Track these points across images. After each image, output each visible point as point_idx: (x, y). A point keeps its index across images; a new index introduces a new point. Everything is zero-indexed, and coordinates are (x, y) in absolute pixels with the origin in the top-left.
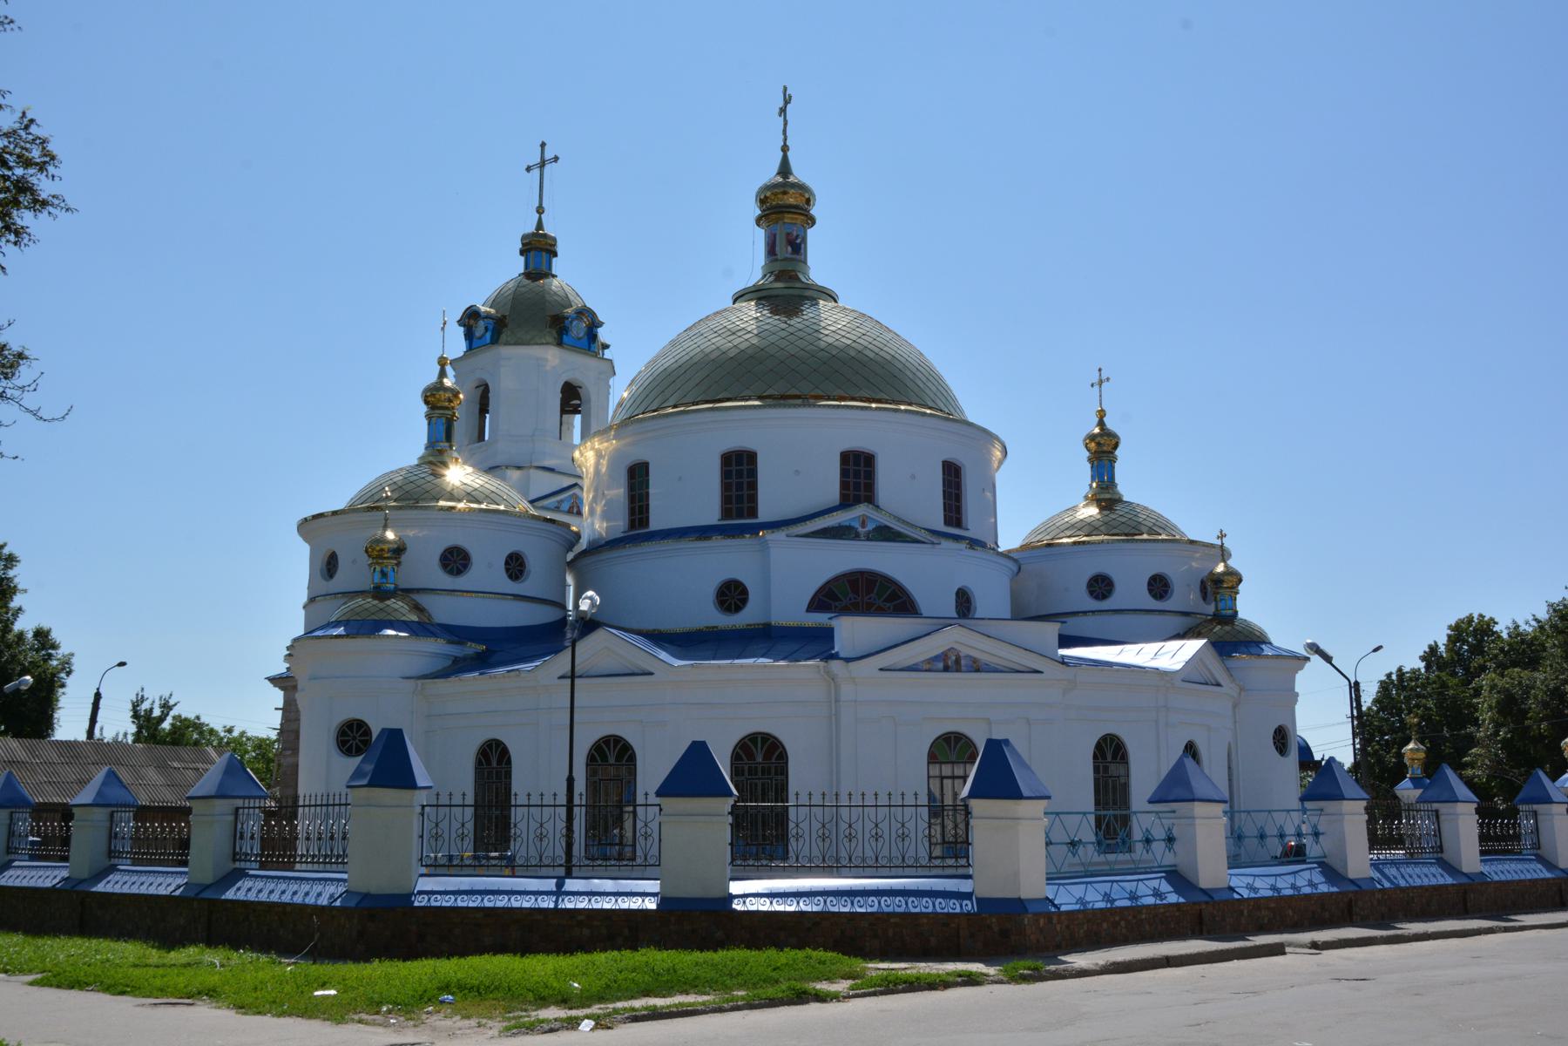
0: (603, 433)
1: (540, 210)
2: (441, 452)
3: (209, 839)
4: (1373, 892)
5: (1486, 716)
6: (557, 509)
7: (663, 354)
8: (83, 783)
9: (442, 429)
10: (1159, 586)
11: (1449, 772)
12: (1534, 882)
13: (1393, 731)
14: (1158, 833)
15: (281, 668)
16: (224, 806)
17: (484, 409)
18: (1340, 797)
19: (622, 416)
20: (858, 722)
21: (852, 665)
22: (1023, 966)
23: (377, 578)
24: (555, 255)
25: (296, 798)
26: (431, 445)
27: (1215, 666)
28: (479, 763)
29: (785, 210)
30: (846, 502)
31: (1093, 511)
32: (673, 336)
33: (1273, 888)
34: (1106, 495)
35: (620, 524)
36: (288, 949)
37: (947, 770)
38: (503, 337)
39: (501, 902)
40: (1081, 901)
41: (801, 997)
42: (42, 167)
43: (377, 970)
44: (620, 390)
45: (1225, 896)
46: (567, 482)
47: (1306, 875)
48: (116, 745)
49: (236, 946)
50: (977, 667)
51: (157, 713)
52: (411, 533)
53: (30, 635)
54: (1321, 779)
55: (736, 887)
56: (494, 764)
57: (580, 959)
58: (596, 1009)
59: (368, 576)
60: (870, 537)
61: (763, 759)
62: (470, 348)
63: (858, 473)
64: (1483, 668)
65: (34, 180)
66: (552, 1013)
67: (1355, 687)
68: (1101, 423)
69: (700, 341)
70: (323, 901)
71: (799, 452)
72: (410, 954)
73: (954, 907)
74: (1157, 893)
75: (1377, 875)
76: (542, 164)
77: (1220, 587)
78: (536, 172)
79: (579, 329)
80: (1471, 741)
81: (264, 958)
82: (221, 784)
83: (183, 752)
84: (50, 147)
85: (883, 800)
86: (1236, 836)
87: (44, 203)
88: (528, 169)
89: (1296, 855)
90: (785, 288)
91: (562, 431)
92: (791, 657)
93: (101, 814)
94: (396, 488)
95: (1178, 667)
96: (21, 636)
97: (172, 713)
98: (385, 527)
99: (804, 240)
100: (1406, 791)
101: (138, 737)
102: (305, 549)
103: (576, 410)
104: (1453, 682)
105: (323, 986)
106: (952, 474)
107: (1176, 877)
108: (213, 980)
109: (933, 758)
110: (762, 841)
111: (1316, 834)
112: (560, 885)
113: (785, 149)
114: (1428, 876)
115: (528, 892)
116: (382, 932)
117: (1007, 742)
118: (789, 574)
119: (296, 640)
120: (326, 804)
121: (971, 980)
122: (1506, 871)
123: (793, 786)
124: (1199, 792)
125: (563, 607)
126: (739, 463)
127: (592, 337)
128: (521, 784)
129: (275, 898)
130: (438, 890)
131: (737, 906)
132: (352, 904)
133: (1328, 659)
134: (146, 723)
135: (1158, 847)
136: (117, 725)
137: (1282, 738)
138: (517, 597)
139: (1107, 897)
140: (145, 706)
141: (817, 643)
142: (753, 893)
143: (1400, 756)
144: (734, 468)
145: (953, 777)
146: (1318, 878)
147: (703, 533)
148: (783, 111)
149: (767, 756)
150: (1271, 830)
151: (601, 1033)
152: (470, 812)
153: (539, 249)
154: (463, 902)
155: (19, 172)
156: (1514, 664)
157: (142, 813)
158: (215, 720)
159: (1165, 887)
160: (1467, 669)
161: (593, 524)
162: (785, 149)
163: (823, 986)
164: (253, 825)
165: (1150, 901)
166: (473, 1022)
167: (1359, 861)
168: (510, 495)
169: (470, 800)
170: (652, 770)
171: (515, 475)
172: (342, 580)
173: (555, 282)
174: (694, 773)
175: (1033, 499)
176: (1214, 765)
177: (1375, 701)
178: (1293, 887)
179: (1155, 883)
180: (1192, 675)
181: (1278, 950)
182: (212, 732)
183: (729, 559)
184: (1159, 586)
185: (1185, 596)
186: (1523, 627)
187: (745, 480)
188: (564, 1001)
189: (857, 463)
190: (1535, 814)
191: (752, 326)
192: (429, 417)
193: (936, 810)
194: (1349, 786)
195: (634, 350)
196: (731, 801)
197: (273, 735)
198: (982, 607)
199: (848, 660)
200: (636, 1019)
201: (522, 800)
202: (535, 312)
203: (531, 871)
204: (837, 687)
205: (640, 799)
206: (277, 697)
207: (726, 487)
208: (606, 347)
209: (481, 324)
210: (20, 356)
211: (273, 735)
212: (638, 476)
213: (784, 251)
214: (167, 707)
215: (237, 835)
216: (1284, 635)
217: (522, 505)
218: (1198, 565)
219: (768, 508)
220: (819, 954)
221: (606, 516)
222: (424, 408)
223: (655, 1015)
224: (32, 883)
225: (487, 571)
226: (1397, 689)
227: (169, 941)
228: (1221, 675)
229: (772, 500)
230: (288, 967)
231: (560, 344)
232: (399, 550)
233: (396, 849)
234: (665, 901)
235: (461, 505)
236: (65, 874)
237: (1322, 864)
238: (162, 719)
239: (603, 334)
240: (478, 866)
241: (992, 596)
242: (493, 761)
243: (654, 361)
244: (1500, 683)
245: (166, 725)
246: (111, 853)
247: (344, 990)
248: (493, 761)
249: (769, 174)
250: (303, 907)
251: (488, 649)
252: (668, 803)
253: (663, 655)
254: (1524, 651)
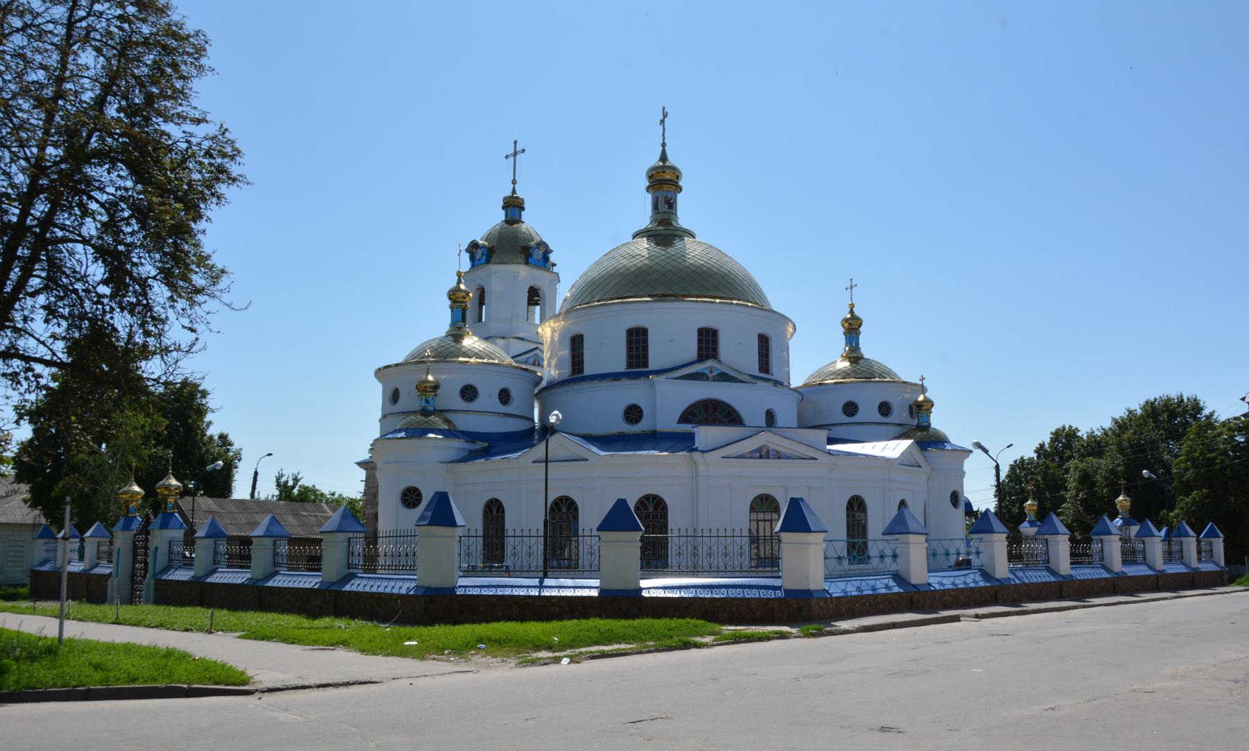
0: (555, 317)
1: (514, 182)
2: (460, 328)
3: (333, 559)
4: (1009, 586)
5: (1071, 485)
6: (526, 362)
7: (591, 270)
8: (256, 524)
9: (459, 314)
10: (885, 409)
11: (1054, 517)
12: (1099, 580)
13: (1016, 494)
14: (888, 552)
15: (366, 456)
16: (342, 537)
17: (481, 303)
18: (992, 531)
19: (567, 306)
20: (710, 487)
21: (706, 455)
22: (812, 628)
23: (423, 403)
25: (376, 531)
26: (453, 324)
27: (918, 455)
28: (485, 512)
29: (664, 183)
30: (701, 358)
31: (847, 364)
32: (597, 258)
33: (953, 584)
34: (854, 355)
35: (567, 372)
36: (384, 619)
37: (761, 516)
38: (493, 259)
39: (508, 592)
40: (844, 591)
41: (686, 646)
42: (232, 158)
43: (439, 631)
44: (563, 292)
45: (926, 588)
46: (532, 346)
47: (972, 576)
48: (266, 502)
49: (353, 617)
50: (779, 456)
51: (291, 483)
52: (442, 377)
53: (216, 438)
54: (979, 522)
55: (644, 583)
57: (555, 625)
58: (568, 652)
59: (418, 402)
60: (715, 379)
61: (653, 510)
62: (473, 266)
63: (708, 341)
64: (1071, 457)
65: (228, 166)
66: (544, 654)
67: (997, 467)
68: (852, 312)
69: (613, 262)
70: (403, 591)
71: (673, 328)
72: (455, 622)
73: (771, 594)
74: (887, 587)
75: (1011, 576)
76: (515, 154)
77: (921, 409)
78: (512, 159)
79: (538, 254)
80: (1064, 500)
81: (370, 624)
82: (340, 525)
83: (309, 506)
84: (237, 145)
85: (714, 533)
86: (932, 555)
87: (234, 180)
88: (507, 157)
89: (964, 565)
90: (664, 229)
91: (529, 316)
92: (672, 450)
93: (268, 541)
94: (434, 350)
95: (896, 456)
96: (211, 438)
98: (427, 373)
99: (675, 201)
100: (1026, 528)
101: (280, 498)
102: (380, 386)
103: (536, 304)
104: (1052, 465)
105: (409, 639)
106: (764, 341)
107: (898, 578)
108: (345, 636)
109: (753, 509)
110: (655, 558)
111: (978, 553)
112: (541, 582)
113: (664, 145)
114: (1039, 576)
115: (524, 587)
116: (436, 611)
117: (802, 499)
118: (667, 401)
119: (376, 440)
120: (396, 536)
121: (783, 636)
122: (1085, 574)
123: (670, 525)
124: (911, 530)
125: (533, 420)
126: (637, 335)
127: (546, 259)
128: (511, 523)
129: (374, 590)
130: (470, 585)
131: (645, 594)
132: (421, 593)
133: (986, 451)
134: (285, 490)
135: (888, 560)
136: (268, 490)
137: (955, 498)
138: (506, 415)
139: (858, 589)
140: (283, 479)
141: (684, 442)
142: (654, 586)
143: (1022, 508)
144: (634, 338)
145: (765, 521)
146: (978, 578)
147: (616, 376)
148: (662, 122)
149: (656, 508)
150: (952, 551)
151: (574, 666)
152: (480, 540)
153: (513, 206)
154: (485, 592)
155: (219, 160)
156: (1090, 455)
157: (293, 541)
158: (325, 487)
159: (892, 583)
160: (1061, 459)
161: (550, 371)
162: (664, 145)
163: (698, 639)
164: (359, 548)
165: (884, 591)
166: (499, 659)
167: (1002, 568)
168: (500, 354)
169: (480, 533)
170: (590, 518)
171: (502, 342)
172: (402, 405)
173: (524, 226)
174: (618, 518)
175: (811, 357)
176: (915, 510)
177: (1007, 476)
178: (965, 583)
179: (886, 581)
180: (905, 462)
181: (956, 619)
182: (322, 495)
183: (632, 392)
184: (885, 409)
185: (900, 415)
186: (1097, 433)
187: (634, 345)
188: (550, 648)
190: (1102, 541)
191: (645, 253)
192: (452, 308)
193: (754, 540)
194: (997, 524)
195: (572, 266)
196: (640, 534)
197: (359, 496)
198: (781, 421)
199: (703, 452)
200: (593, 658)
201: (510, 533)
202: (511, 246)
203: (524, 574)
204: (697, 468)
205: (580, 533)
206: (362, 474)
207: (629, 349)
208: (554, 265)
209: (480, 251)
210: (223, 271)
211: (359, 496)
212: (577, 343)
213: (663, 207)
214: (296, 480)
215: (350, 554)
216: (957, 437)
217: (508, 360)
218: (908, 397)
219: (654, 362)
220: (694, 621)
221: (558, 366)
222: (449, 302)
223: (604, 655)
224: (230, 581)
225: (488, 398)
226: (1020, 467)
227: (314, 614)
228: (922, 462)
229: (656, 358)
230: (387, 629)
231: (527, 263)
232: (436, 387)
233: (446, 562)
234: (603, 591)
235: (473, 360)
236: (249, 576)
237: (980, 570)
238: (293, 487)
239: (553, 258)
240: (488, 570)
241: (787, 414)
242: (494, 510)
243: (586, 274)
244: (1081, 465)
245: (295, 491)
246: (275, 564)
247: (421, 642)
248: (494, 510)
249: (654, 160)
250: (391, 595)
251: (491, 445)
252: (602, 534)
253: (594, 449)
254: (1095, 446)
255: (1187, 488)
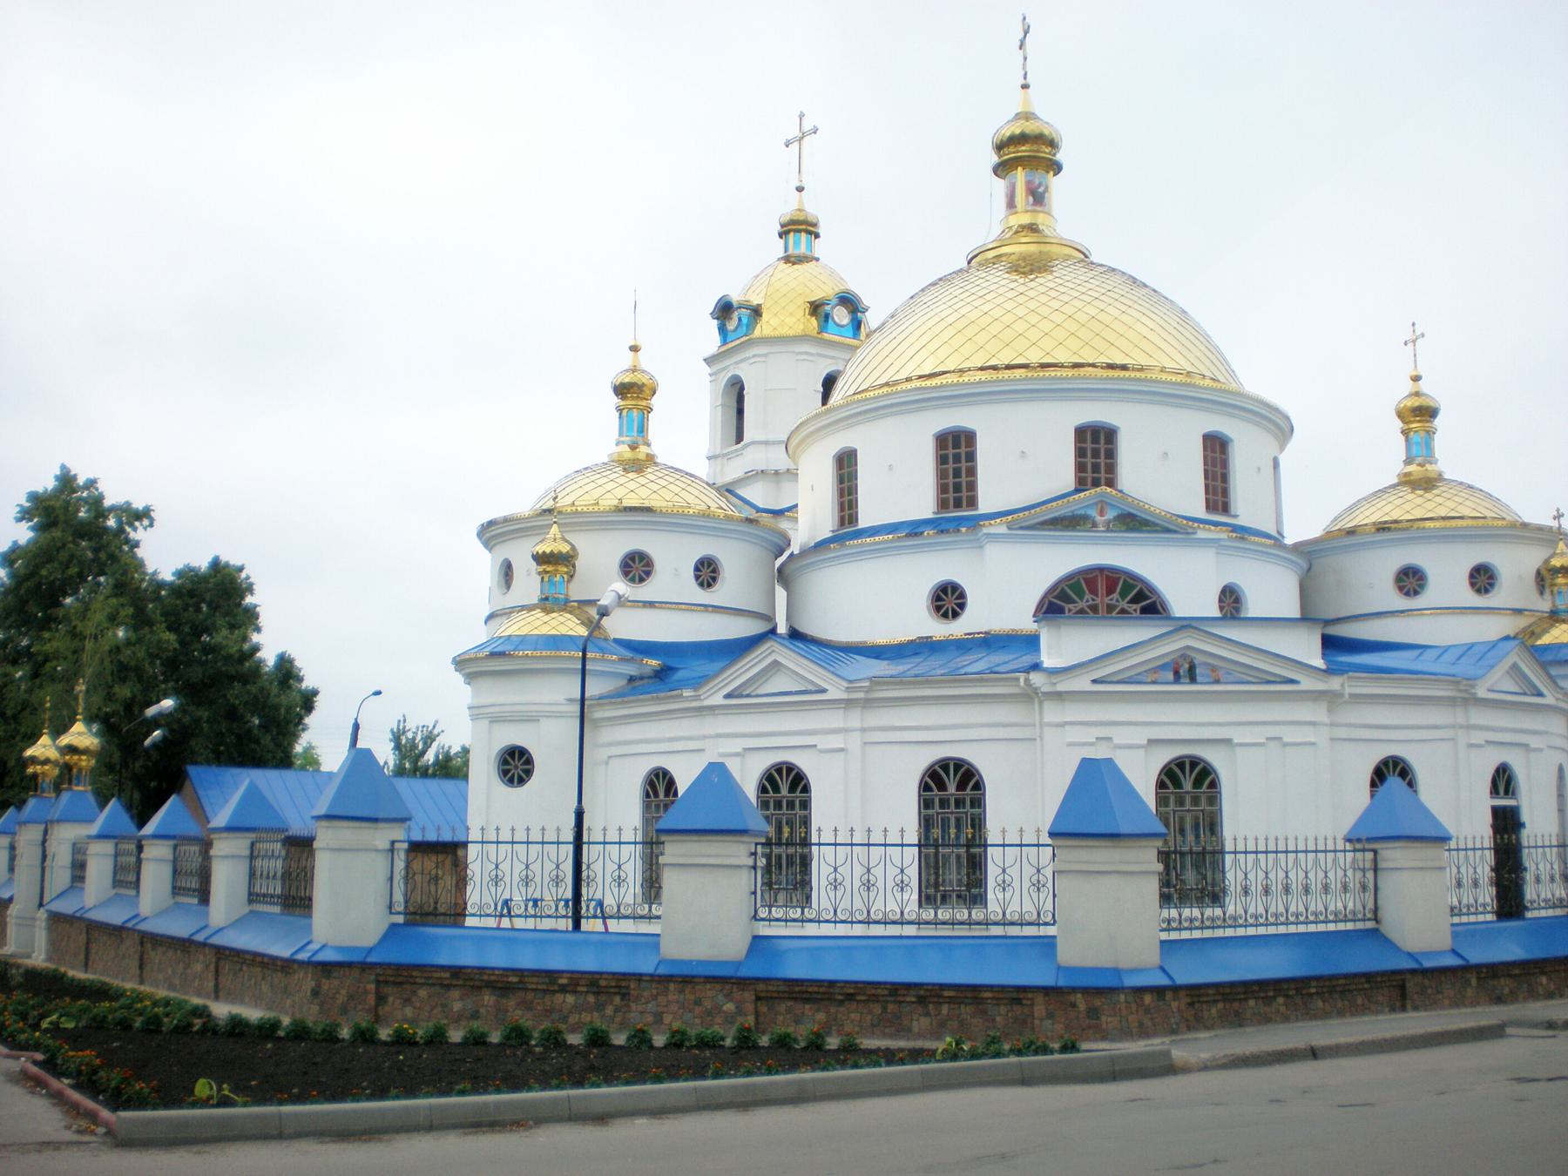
24: (817, 236)
56: (662, 796)
97: (435, 745)
125: (770, 618)
126: (956, 445)
144: (951, 452)
147: (913, 530)
148: (1026, 33)
149: (961, 786)
169: (1228, 859)
189: (1095, 440)
205: (814, 839)
207: (941, 475)
219: (988, 500)
229: (992, 494)
255: (30, 691)
